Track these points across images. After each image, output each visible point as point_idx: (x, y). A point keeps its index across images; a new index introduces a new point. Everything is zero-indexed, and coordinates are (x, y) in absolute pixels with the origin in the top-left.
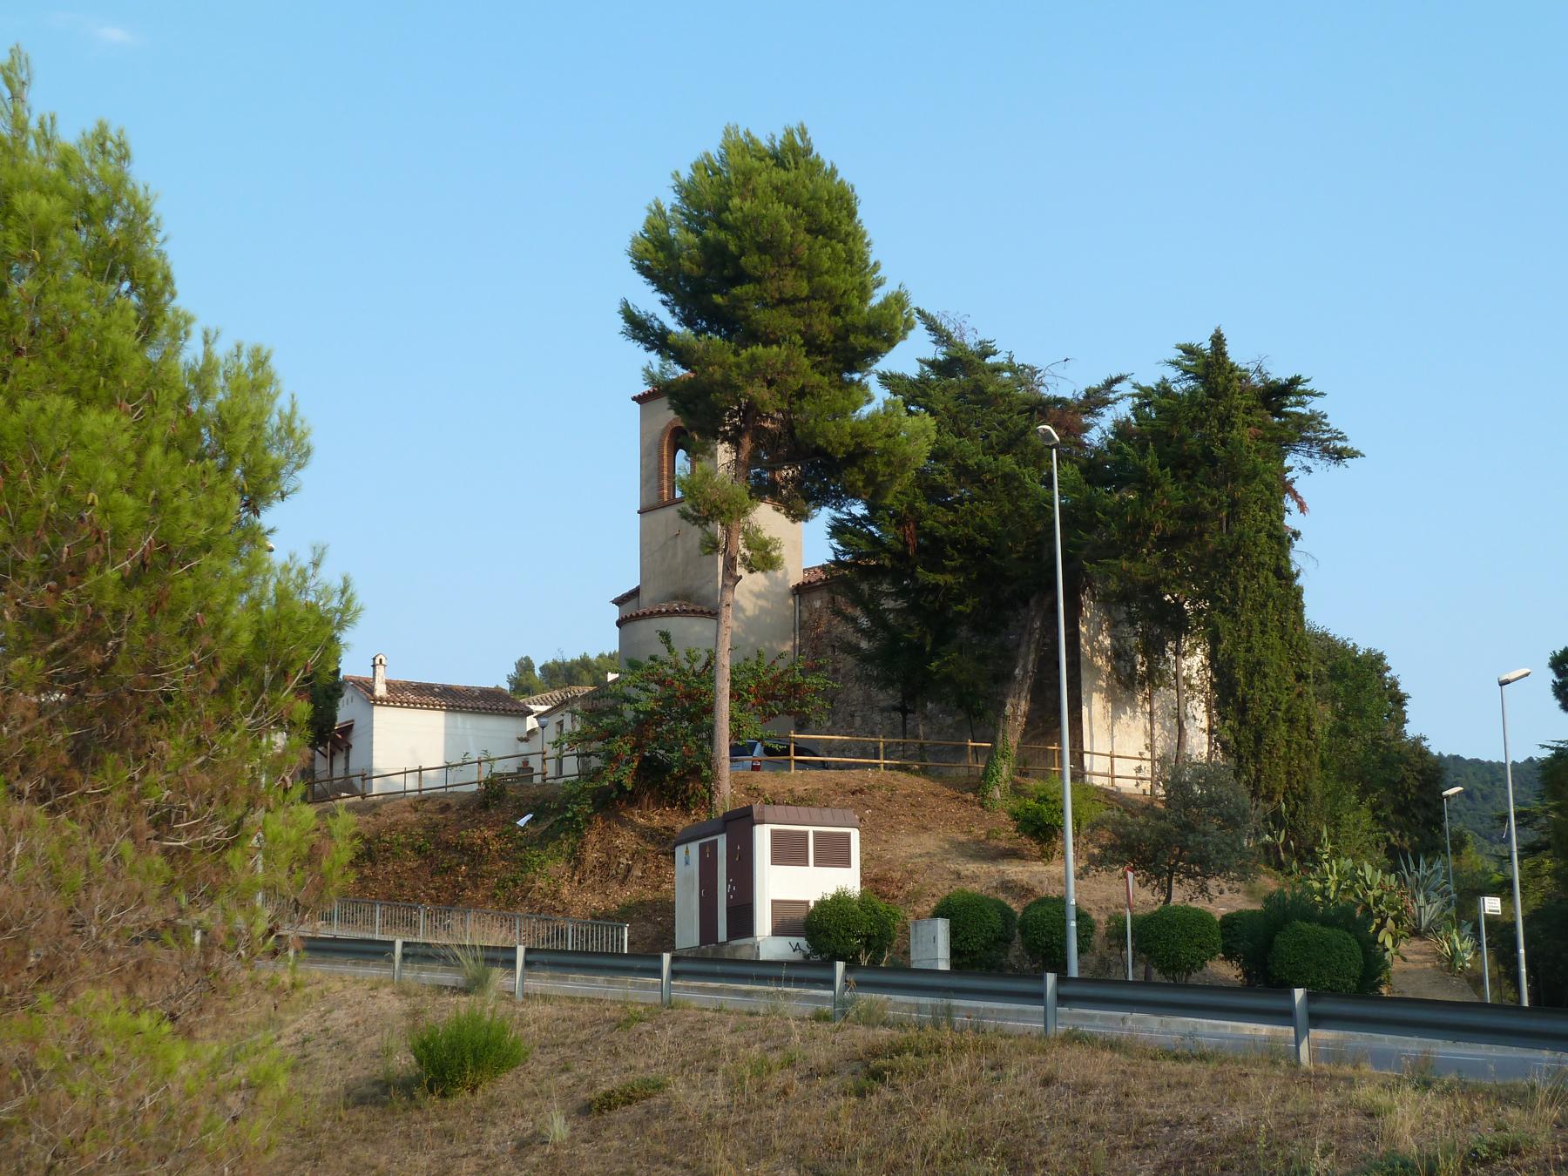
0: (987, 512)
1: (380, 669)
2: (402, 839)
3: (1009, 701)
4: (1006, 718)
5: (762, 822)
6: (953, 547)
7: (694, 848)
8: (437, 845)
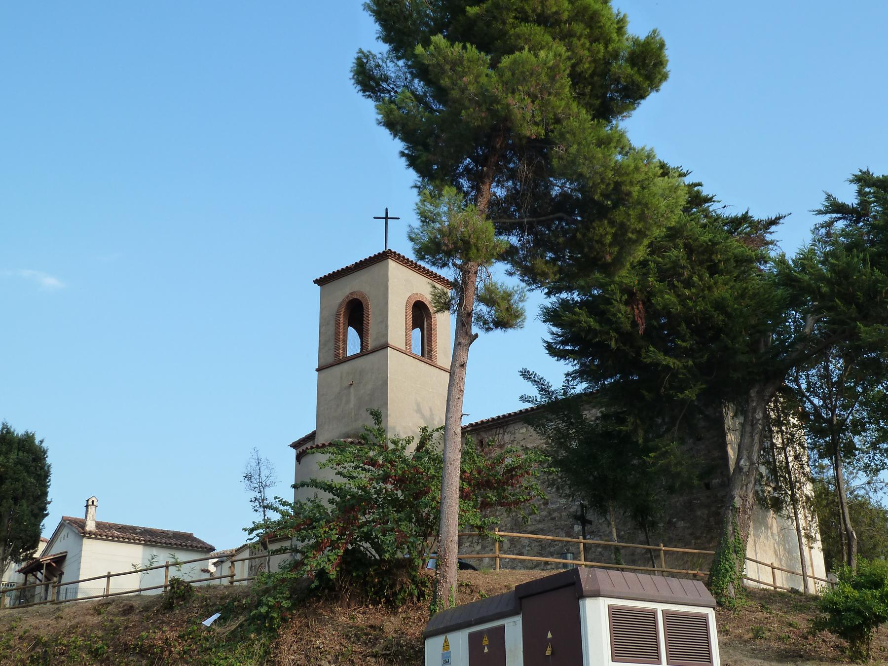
0: (722, 291)
1: (92, 509)
2: (80, 642)
3: (737, 493)
4: (736, 510)
5: (597, 594)
6: (688, 325)
7: (459, 641)
8: (115, 647)
